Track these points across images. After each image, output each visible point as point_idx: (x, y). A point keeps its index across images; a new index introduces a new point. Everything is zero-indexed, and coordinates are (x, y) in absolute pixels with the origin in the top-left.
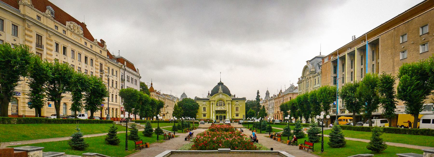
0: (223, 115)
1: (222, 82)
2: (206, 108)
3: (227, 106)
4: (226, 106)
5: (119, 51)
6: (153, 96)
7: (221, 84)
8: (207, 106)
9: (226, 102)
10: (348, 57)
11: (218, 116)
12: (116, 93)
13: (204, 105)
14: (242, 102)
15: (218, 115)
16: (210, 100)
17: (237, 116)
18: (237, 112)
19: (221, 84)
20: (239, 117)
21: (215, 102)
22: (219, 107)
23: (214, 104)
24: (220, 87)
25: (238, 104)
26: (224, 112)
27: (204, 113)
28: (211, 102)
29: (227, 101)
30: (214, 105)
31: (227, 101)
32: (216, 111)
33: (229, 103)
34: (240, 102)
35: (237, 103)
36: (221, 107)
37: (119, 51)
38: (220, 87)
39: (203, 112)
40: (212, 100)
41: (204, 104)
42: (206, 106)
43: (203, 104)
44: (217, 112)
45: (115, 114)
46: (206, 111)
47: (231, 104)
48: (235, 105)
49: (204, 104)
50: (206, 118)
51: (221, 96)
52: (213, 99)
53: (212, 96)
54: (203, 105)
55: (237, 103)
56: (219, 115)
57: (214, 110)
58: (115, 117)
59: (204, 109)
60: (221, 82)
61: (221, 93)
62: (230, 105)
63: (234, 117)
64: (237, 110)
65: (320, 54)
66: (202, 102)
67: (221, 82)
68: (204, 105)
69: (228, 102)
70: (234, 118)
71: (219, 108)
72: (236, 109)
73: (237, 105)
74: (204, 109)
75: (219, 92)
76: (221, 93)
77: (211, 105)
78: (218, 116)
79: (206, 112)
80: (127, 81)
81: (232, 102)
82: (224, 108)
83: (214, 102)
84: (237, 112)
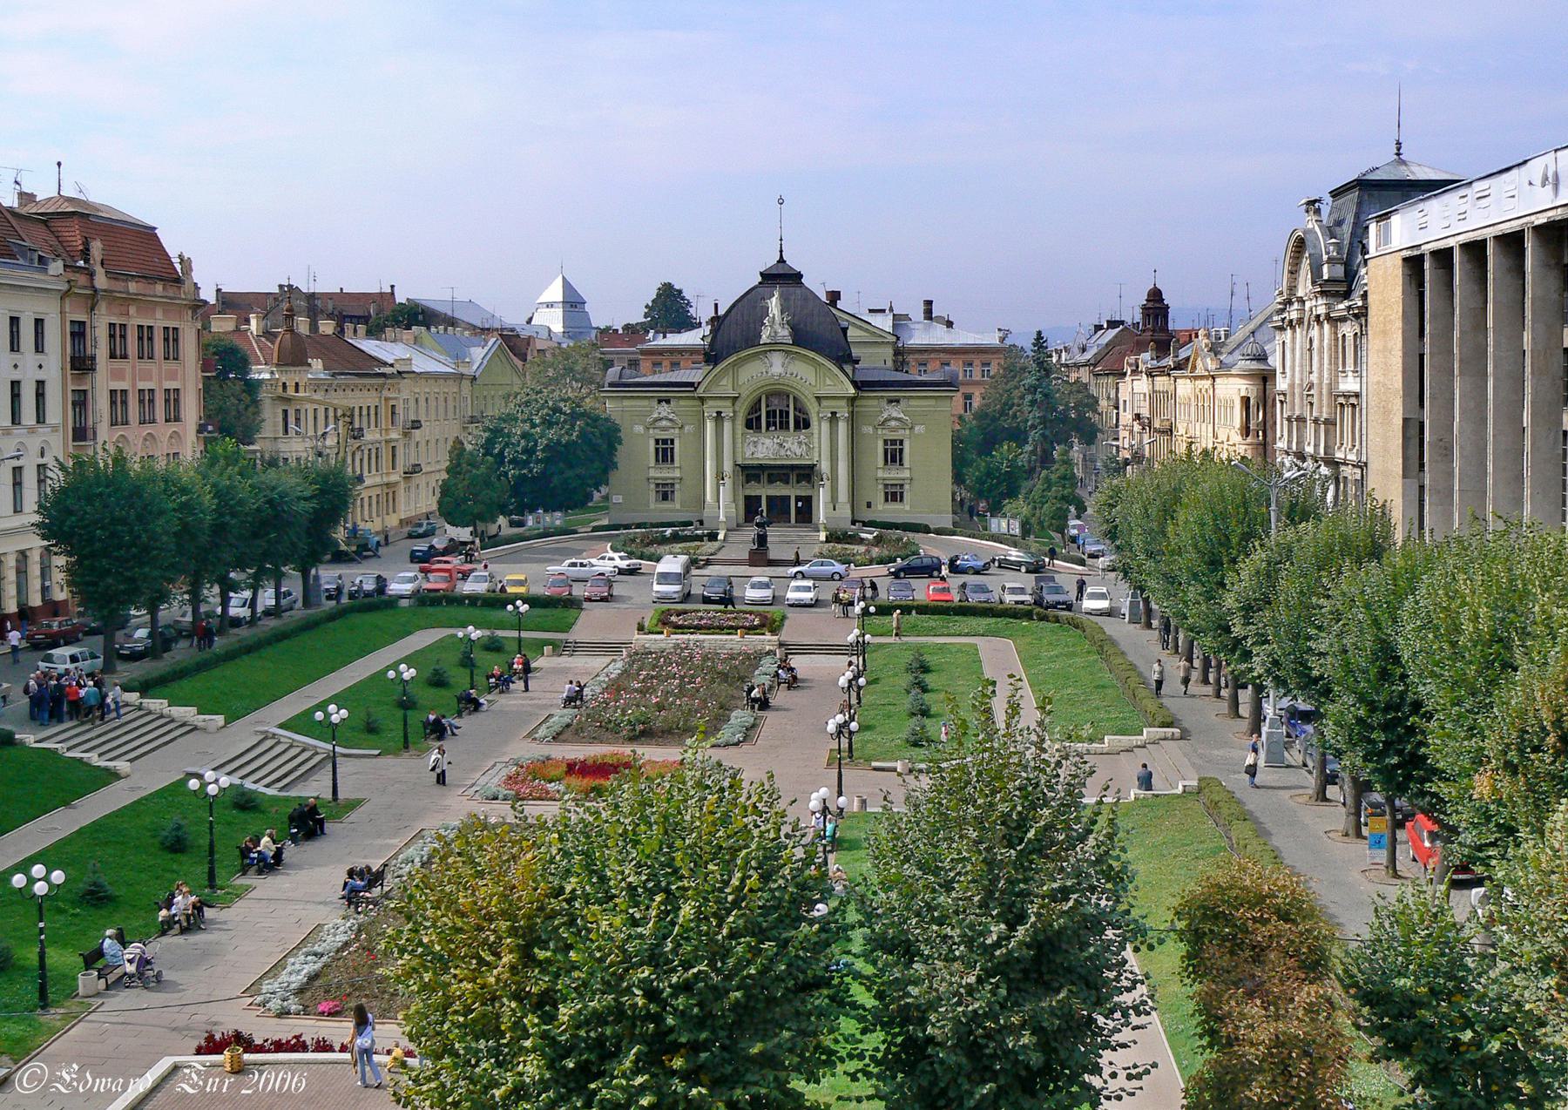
0: (791, 491)
1: (794, 262)
2: (677, 442)
3: (819, 429)
4: (816, 431)
5: (59, 164)
6: (301, 389)
7: (781, 277)
8: (682, 428)
9: (813, 409)
10: (1469, 266)
11: (759, 498)
12: (42, 455)
13: (664, 423)
14: (932, 402)
15: (757, 493)
16: (701, 389)
17: (894, 499)
18: (893, 474)
19: (781, 277)
20: (907, 508)
21: (738, 404)
22: (763, 440)
23: (733, 419)
24: (774, 305)
25: (896, 419)
26: (807, 473)
27: (667, 479)
28: (711, 403)
29: (818, 399)
30: (727, 426)
31: (818, 399)
32: (744, 468)
33: (834, 414)
34: (913, 402)
35: (895, 415)
36: (781, 436)
37: (59, 164)
38: (774, 305)
39: (652, 473)
40: (717, 392)
41: (661, 419)
42: (677, 431)
43: (656, 415)
44: (751, 473)
45: (35, 584)
46: (677, 464)
47: (853, 421)
48: (875, 428)
49: (661, 419)
50: (675, 509)
51: (777, 366)
52: (726, 387)
53: (716, 365)
54: (657, 420)
55: (894, 411)
56: (764, 491)
57: (728, 467)
58: (35, 600)
59: (665, 452)
60: (781, 261)
61: (774, 346)
62: (842, 427)
63: (869, 505)
64: (894, 456)
65: (1398, 154)
66: (646, 403)
67: (781, 261)
68: (664, 423)
69: (824, 403)
70: (868, 515)
71: (767, 441)
72: (886, 451)
73: (893, 423)
74: (665, 452)
75: (765, 337)
76: (774, 346)
77: (710, 426)
78: (759, 498)
79: (677, 474)
80: (112, 356)
81: (858, 403)
82: (800, 443)
83: (729, 403)
84: (893, 474)
